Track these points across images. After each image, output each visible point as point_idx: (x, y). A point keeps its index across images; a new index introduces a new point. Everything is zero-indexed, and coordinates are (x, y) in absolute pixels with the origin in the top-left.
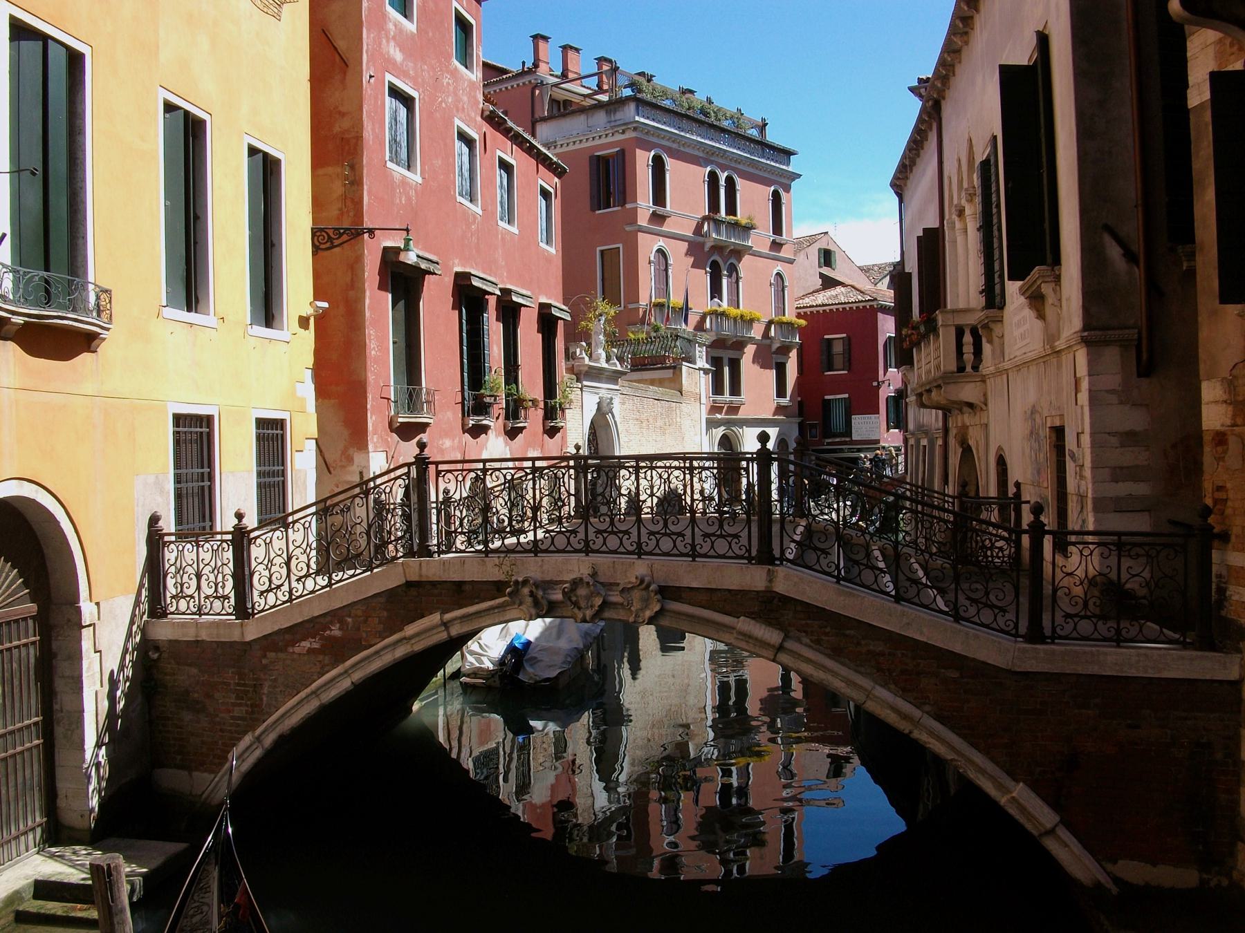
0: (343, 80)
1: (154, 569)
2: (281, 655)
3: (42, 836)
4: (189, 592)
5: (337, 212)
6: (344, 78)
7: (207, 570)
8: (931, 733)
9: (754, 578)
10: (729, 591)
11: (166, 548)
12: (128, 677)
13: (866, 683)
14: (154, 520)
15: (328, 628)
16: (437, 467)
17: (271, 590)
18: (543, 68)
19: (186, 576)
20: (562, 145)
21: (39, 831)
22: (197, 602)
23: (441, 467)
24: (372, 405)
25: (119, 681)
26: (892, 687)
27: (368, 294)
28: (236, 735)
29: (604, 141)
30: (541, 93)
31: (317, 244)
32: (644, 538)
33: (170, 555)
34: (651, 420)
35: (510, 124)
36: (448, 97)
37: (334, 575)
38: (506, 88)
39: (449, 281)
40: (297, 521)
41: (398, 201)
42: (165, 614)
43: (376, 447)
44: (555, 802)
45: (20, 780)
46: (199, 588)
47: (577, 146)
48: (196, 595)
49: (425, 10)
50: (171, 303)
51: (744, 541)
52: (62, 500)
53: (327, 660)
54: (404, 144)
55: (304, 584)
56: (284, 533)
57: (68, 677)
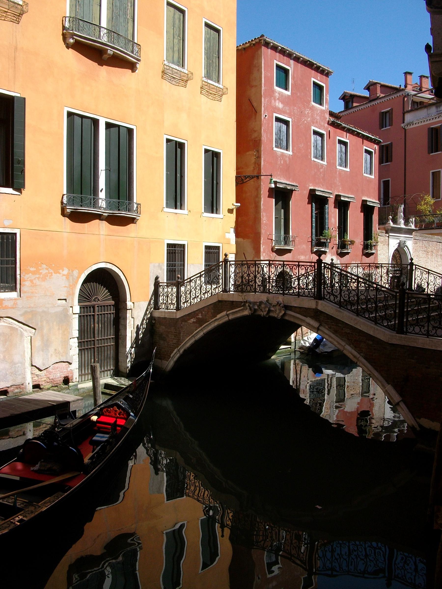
0: (255, 118)
1: (156, 294)
2: (186, 323)
3: (113, 373)
5: (252, 169)
10: (306, 308)
12: (144, 328)
13: (343, 343)
15: (198, 315)
16: (230, 263)
18: (409, 87)
19: (173, 297)
20: (416, 124)
21: (112, 371)
24: (263, 242)
25: (141, 328)
26: (352, 346)
27: (262, 199)
29: (435, 120)
30: (408, 100)
31: (238, 182)
34: (434, 251)
35: (344, 125)
36: (308, 118)
38: (392, 98)
39: (306, 193)
41: (279, 163)
42: (159, 309)
44: (359, 412)
45: (106, 354)
47: (423, 124)
49: (296, 85)
50: (168, 206)
53: (197, 325)
54: (285, 140)
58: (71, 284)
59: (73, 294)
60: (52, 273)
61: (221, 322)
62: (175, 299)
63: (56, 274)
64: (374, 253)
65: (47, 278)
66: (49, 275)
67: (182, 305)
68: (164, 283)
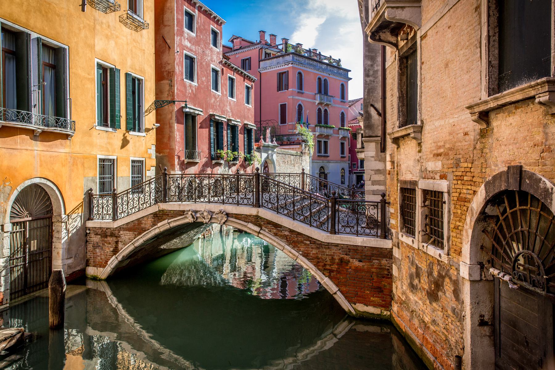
4: (100, 213)
6: (169, 53)
8: (302, 261)
9: (253, 211)
10: (246, 215)
23: (170, 176)
32: (239, 200)
46: (102, 212)
51: (252, 200)
61: (162, 229)
62: (111, 210)
64: (197, 163)
67: (118, 215)
68: (97, 195)
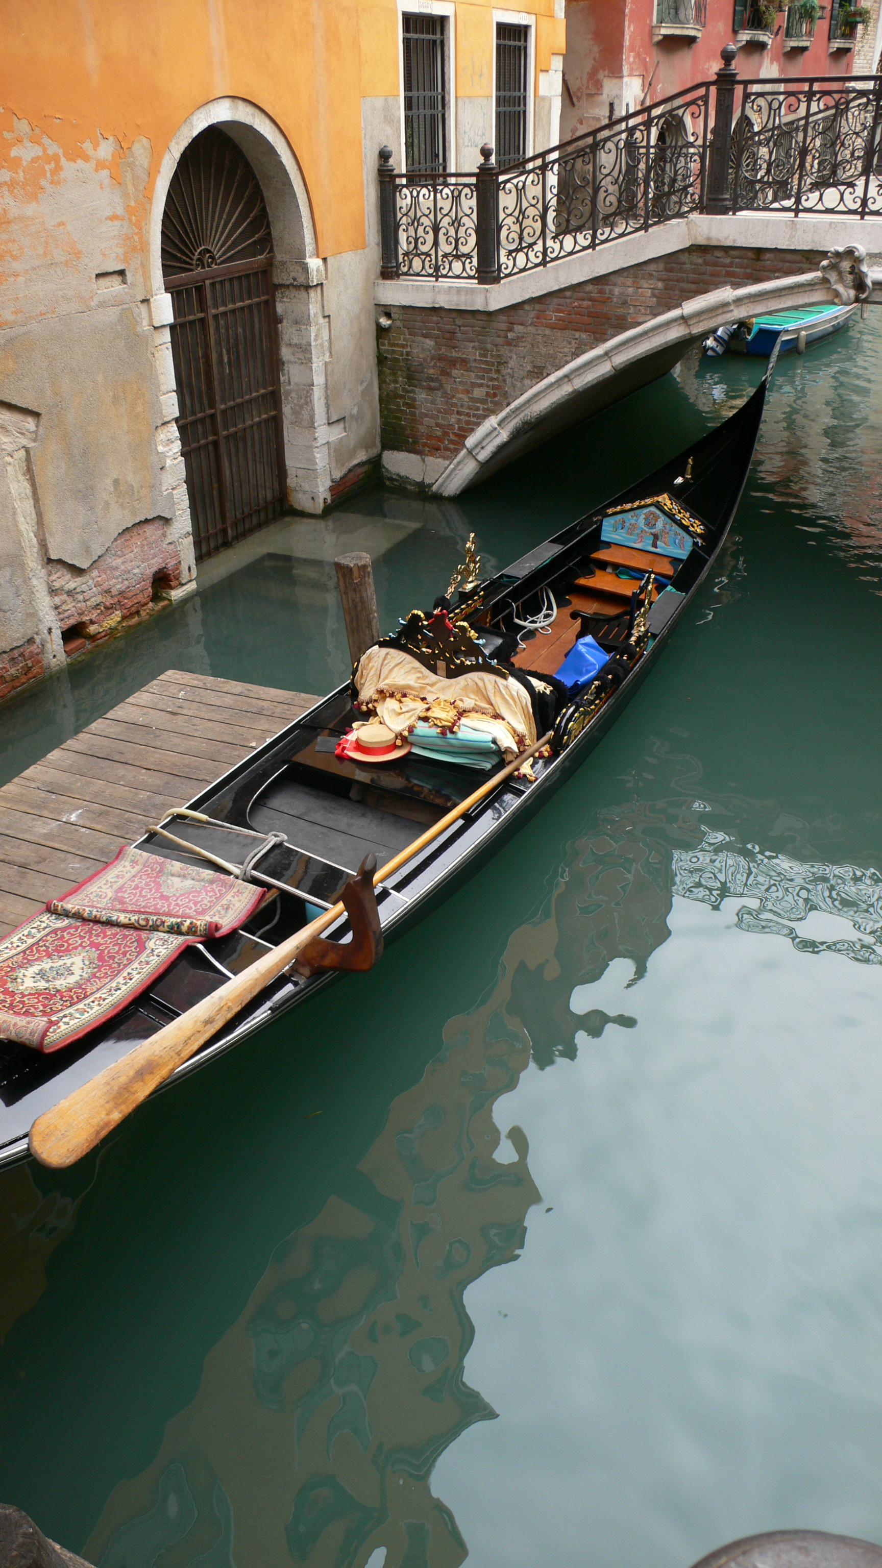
4: (424, 249)
7: (445, 222)
11: (398, 194)
14: (384, 156)
16: (745, 89)
17: (521, 250)
19: (421, 229)
22: (433, 261)
28: (475, 420)
33: (404, 200)
37: (600, 231)
40: (508, 181)
43: (631, 70)
46: (436, 243)
48: (433, 252)
52: (283, 128)
55: (561, 243)
56: (541, 176)
57: (296, 345)
58: (133, 204)
59: (144, 247)
60: (56, 158)
62: (473, 240)
63: (72, 164)
65: (43, 183)
66: (47, 167)
67: (503, 259)
